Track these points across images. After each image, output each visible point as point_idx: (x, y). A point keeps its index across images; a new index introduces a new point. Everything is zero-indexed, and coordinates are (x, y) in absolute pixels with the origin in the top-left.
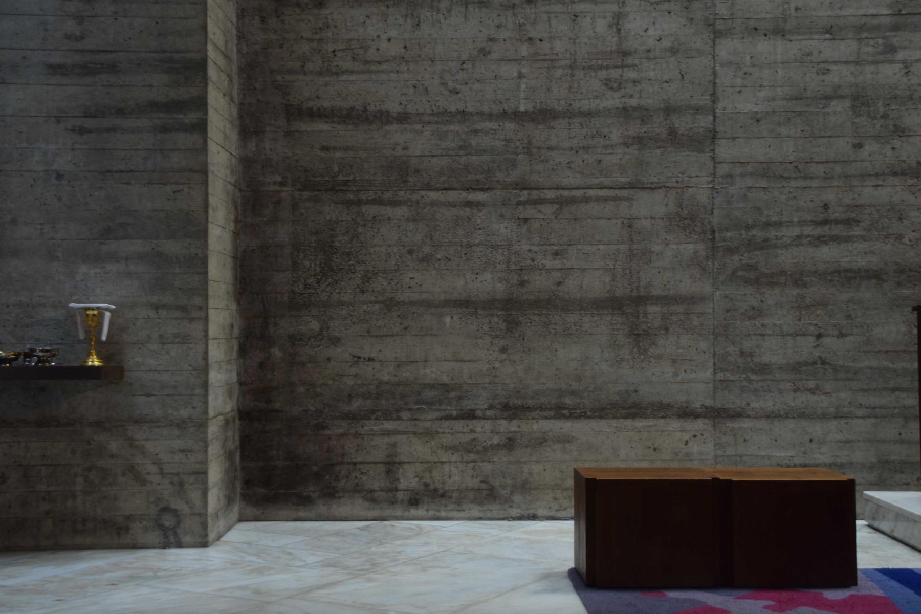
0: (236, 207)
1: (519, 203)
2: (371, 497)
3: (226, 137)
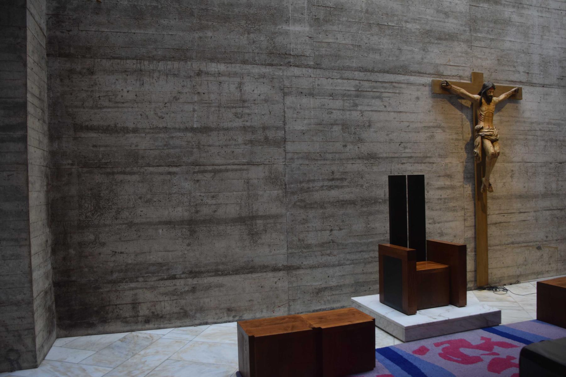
0: (47, 178)
1: (194, 173)
2: (125, 321)
3: (40, 142)
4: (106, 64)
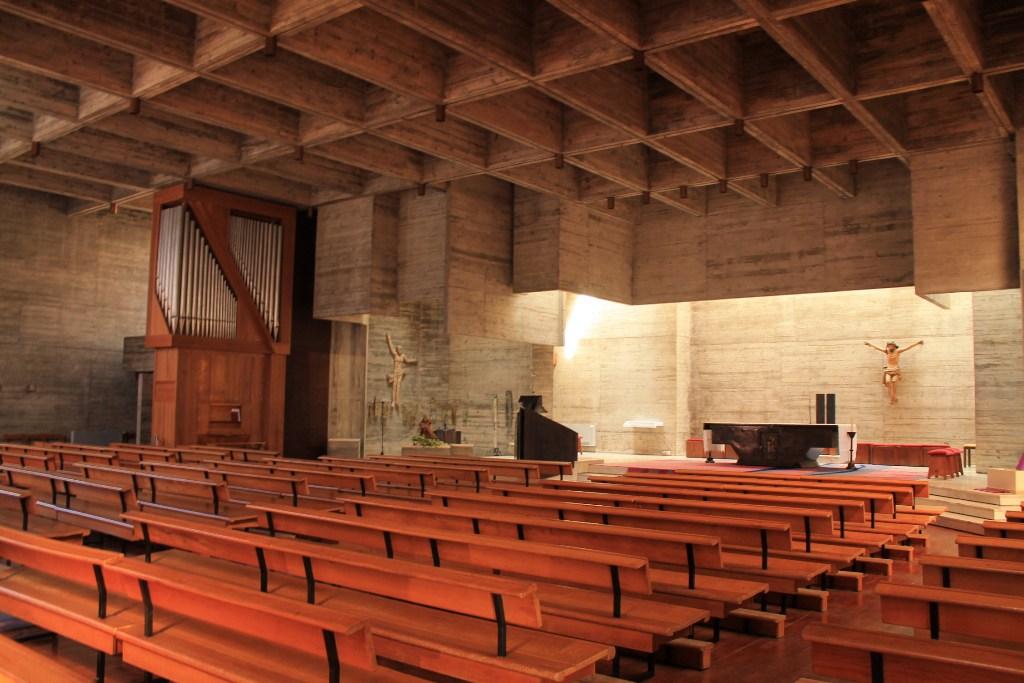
4: (710, 347)
